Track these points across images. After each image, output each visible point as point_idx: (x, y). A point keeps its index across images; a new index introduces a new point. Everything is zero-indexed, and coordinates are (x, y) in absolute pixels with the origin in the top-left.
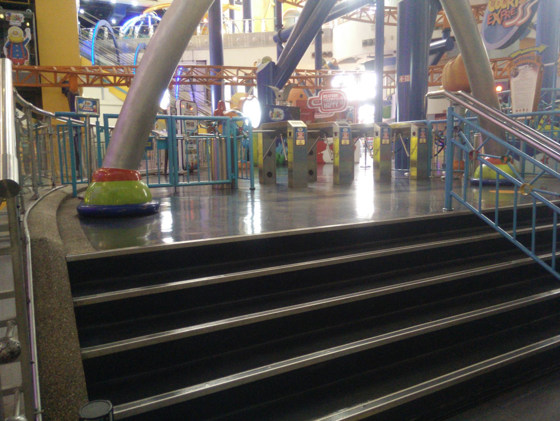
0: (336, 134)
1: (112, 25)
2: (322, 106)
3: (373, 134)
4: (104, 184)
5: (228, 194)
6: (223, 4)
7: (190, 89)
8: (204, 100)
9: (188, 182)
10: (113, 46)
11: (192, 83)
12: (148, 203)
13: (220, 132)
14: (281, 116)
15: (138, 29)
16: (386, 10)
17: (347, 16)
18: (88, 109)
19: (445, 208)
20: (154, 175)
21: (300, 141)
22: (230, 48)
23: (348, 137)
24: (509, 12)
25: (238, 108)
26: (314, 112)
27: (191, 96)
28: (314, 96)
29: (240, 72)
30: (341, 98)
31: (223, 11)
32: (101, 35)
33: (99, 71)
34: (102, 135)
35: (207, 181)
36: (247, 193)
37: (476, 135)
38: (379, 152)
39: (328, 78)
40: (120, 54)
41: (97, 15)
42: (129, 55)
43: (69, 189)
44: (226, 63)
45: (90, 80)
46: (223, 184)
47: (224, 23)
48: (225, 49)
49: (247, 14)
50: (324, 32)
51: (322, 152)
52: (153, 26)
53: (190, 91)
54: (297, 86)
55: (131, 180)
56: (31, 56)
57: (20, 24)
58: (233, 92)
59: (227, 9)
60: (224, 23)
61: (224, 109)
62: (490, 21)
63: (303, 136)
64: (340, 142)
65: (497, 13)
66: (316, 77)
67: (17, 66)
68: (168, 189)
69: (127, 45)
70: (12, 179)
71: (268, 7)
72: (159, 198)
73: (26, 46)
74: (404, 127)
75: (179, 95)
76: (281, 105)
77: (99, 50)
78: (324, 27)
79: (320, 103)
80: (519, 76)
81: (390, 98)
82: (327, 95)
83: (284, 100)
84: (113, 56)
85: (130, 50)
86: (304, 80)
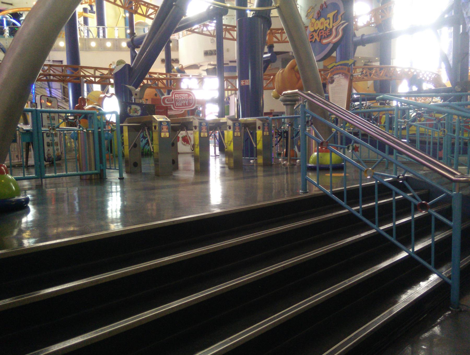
0: (196, 127)
3: (226, 128)
5: (96, 184)
6: (78, 12)
7: (47, 86)
9: (55, 173)
11: (49, 81)
12: (16, 198)
16: (223, 27)
17: (191, 29)
19: (302, 190)
20: (14, 167)
21: (165, 134)
23: (206, 130)
24: (326, 32)
25: (98, 104)
27: (49, 93)
28: (166, 96)
29: (97, 72)
30: (190, 98)
31: (79, 18)
35: (75, 173)
37: (308, 129)
38: (232, 143)
39: (179, 81)
44: (82, 63)
46: (91, 174)
49: (101, 21)
50: (172, 41)
52: (8, 27)
53: (47, 88)
54: (150, 86)
60: (79, 28)
62: (311, 39)
64: (200, 134)
65: (316, 33)
74: (252, 122)
75: (36, 92)
76: (139, 102)
78: (172, 37)
79: (172, 101)
80: (334, 83)
81: (228, 99)
82: (178, 95)
83: (141, 98)
86: (157, 82)
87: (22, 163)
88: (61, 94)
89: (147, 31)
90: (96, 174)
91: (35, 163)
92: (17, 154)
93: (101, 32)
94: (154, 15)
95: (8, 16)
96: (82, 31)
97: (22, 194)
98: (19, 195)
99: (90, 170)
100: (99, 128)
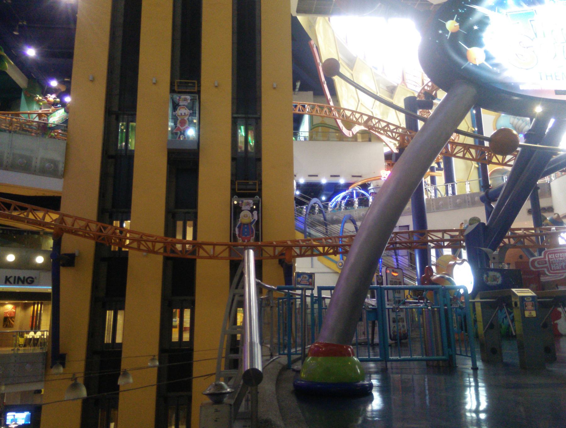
1: (322, 202)
2: (549, 266)
4: (320, 359)
7: (394, 254)
8: (408, 264)
10: (322, 219)
11: (395, 249)
12: (361, 382)
13: (428, 299)
14: (498, 280)
15: (344, 202)
18: (304, 282)
21: (530, 313)
22: (433, 212)
26: (539, 274)
27: (395, 260)
29: (445, 235)
32: (313, 211)
33: (311, 243)
34: (316, 306)
36: (469, 374)
39: (554, 235)
40: (328, 226)
41: (309, 195)
42: (336, 226)
43: (284, 360)
44: (430, 227)
45: (303, 251)
46: (438, 360)
47: (425, 189)
48: (427, 213)
49: (449, 178)
51: (555, 322)
53: (393, 256)
54: (514, 246)
55: (344, 355)
56: (256, 233)
57: (249, 209)
58: (438, 255)
59: (428, 177)
61: (432, 275)
63: (532, 306)
66: (536, 235)
67: (245, 243)
68: (376, 364)
69: (335, 217)
70: (257, 367)
71: (471, 169)
72: (367, 374)
73: (253, 226)
76: (498, 268)
77: (311, 223)
79: (546, 263)
82: (553, 255)
83: (501, 263)
84: (322, 228)
85: (336, 222)
86: (522, 240)
87: (367, 340)
88: (407, 261)
89: (505, 179)
90: (444, 360)
91: (380, 341)
92: (364, 331)
93: (450, 189)
94: (513, 161)
95: (357, 188)
96: (429, 191)
97: (366, 379)
98: (363, 380)
99: (438, 355)
100: (445, 305)
